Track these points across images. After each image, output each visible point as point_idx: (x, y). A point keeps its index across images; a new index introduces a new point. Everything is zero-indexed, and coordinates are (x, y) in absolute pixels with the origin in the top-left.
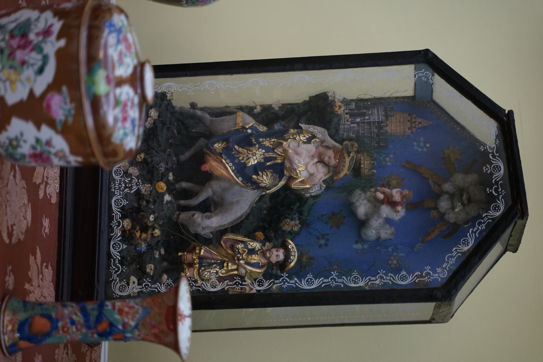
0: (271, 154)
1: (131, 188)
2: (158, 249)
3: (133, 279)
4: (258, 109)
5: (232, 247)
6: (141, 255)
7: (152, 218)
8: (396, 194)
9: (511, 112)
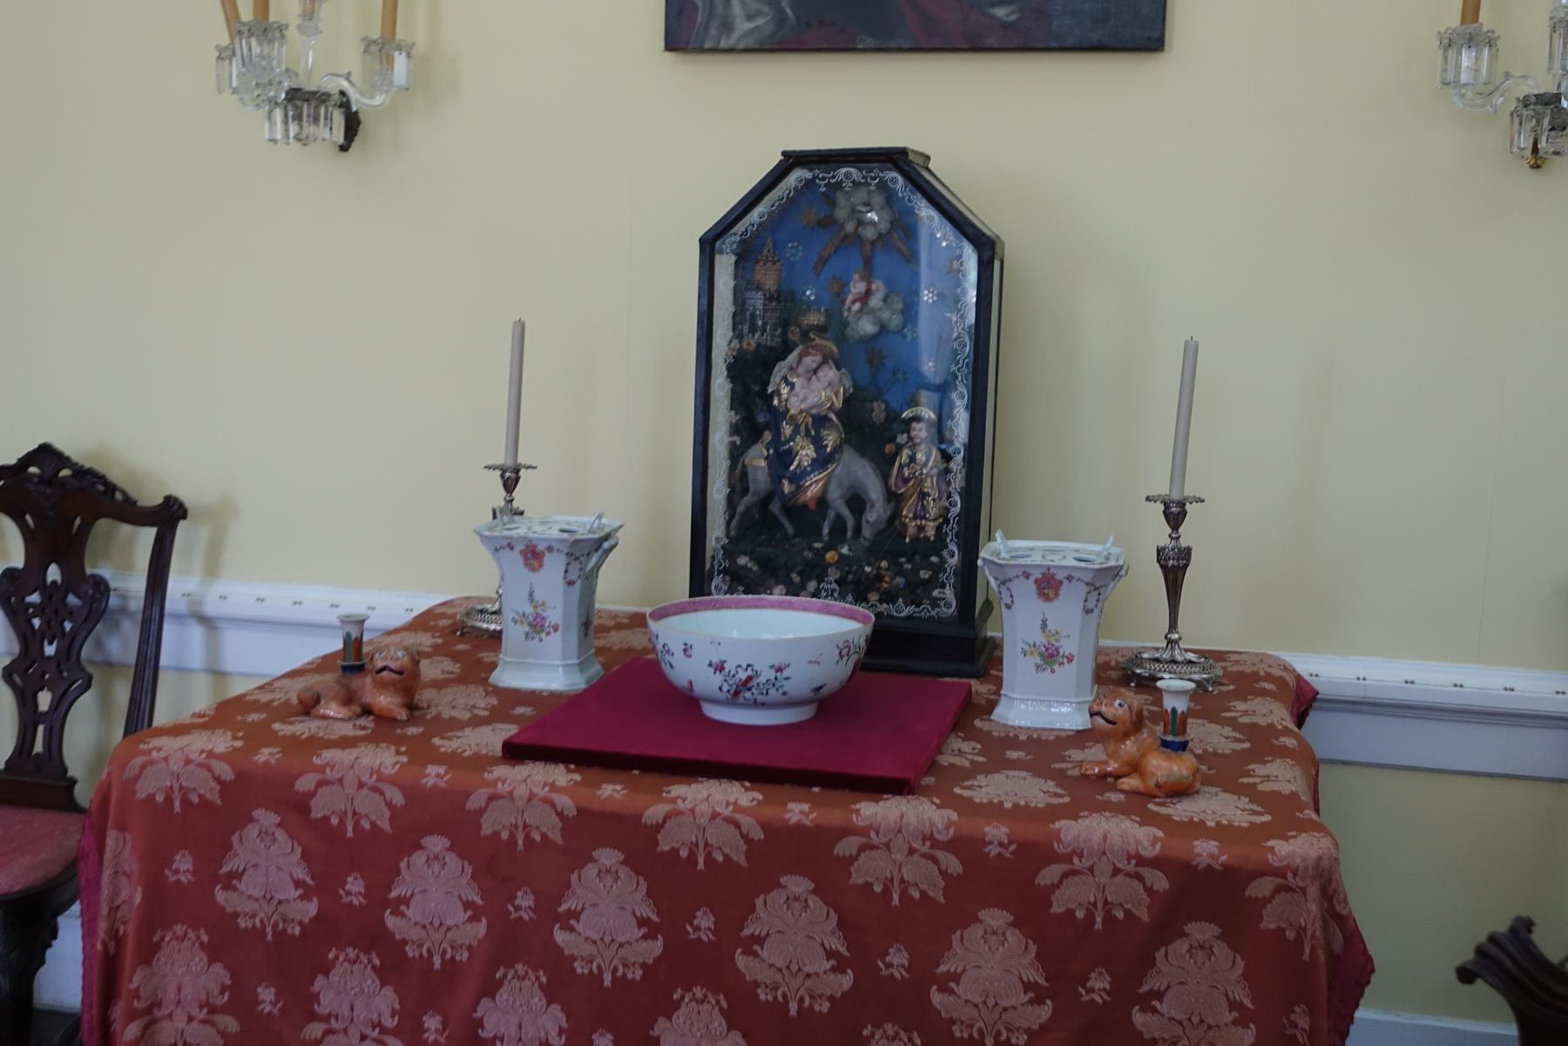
0: (802, 428)
1: (833, 591)
2: (901, 565)
3: (935, 593)
4: (737, 440)
5: (906, 481)
6: (908, 584)
7: (868, 569)
8: (857, 288)
9: (784, 153)
